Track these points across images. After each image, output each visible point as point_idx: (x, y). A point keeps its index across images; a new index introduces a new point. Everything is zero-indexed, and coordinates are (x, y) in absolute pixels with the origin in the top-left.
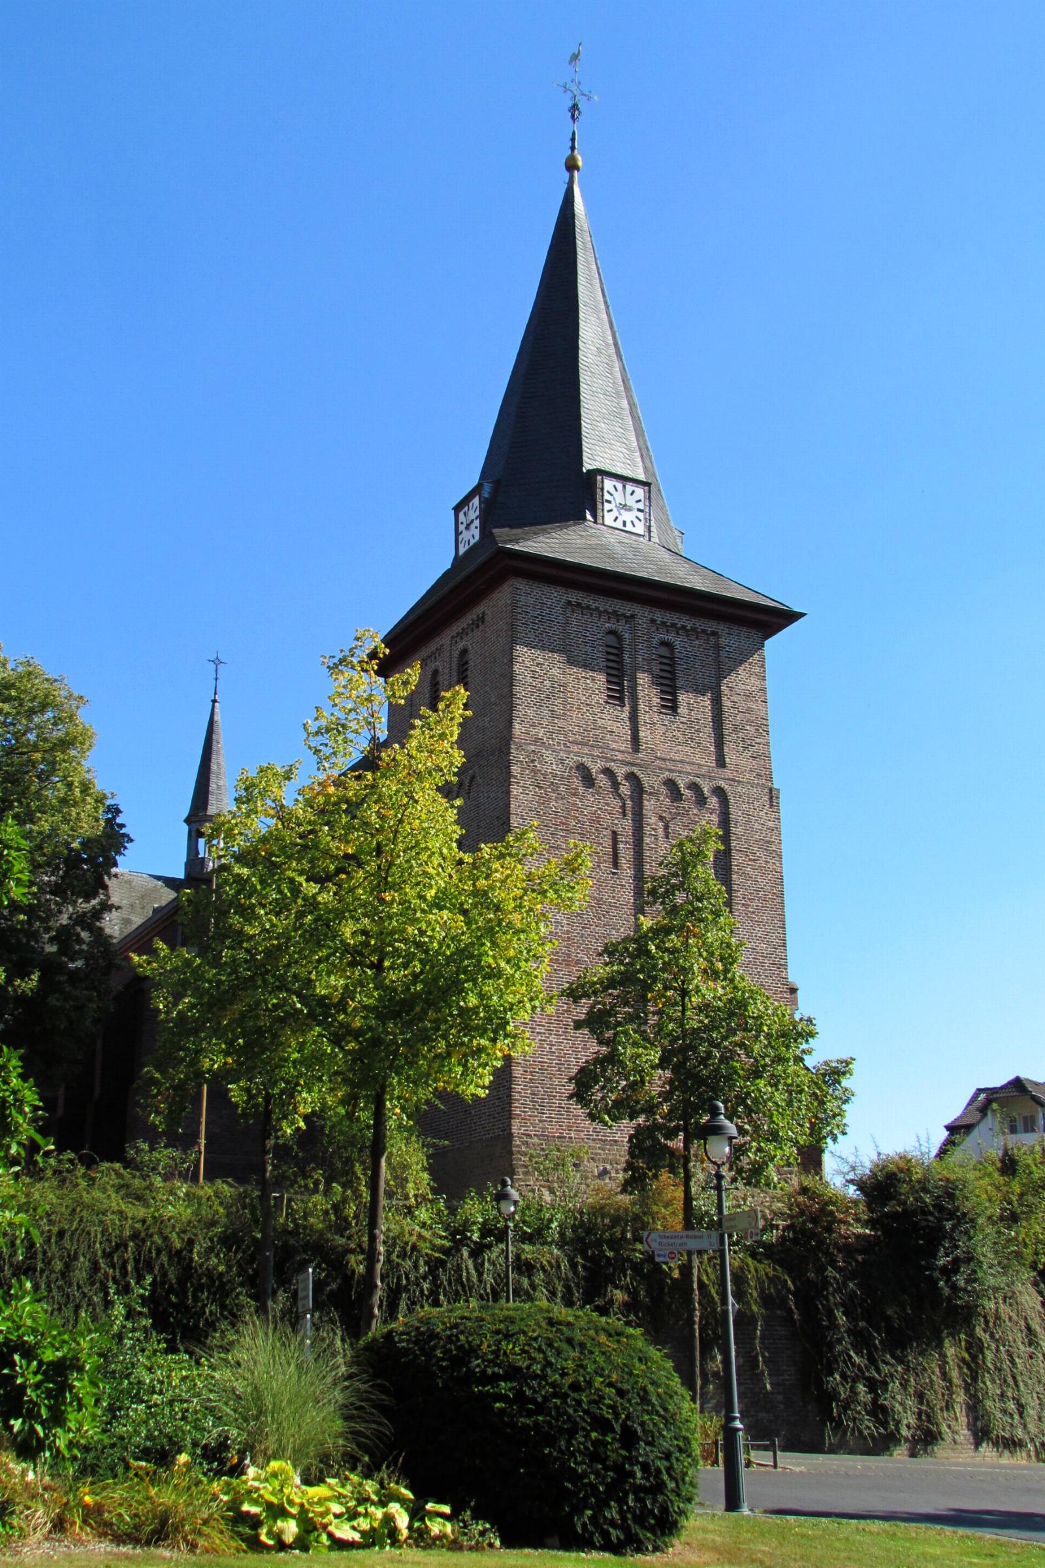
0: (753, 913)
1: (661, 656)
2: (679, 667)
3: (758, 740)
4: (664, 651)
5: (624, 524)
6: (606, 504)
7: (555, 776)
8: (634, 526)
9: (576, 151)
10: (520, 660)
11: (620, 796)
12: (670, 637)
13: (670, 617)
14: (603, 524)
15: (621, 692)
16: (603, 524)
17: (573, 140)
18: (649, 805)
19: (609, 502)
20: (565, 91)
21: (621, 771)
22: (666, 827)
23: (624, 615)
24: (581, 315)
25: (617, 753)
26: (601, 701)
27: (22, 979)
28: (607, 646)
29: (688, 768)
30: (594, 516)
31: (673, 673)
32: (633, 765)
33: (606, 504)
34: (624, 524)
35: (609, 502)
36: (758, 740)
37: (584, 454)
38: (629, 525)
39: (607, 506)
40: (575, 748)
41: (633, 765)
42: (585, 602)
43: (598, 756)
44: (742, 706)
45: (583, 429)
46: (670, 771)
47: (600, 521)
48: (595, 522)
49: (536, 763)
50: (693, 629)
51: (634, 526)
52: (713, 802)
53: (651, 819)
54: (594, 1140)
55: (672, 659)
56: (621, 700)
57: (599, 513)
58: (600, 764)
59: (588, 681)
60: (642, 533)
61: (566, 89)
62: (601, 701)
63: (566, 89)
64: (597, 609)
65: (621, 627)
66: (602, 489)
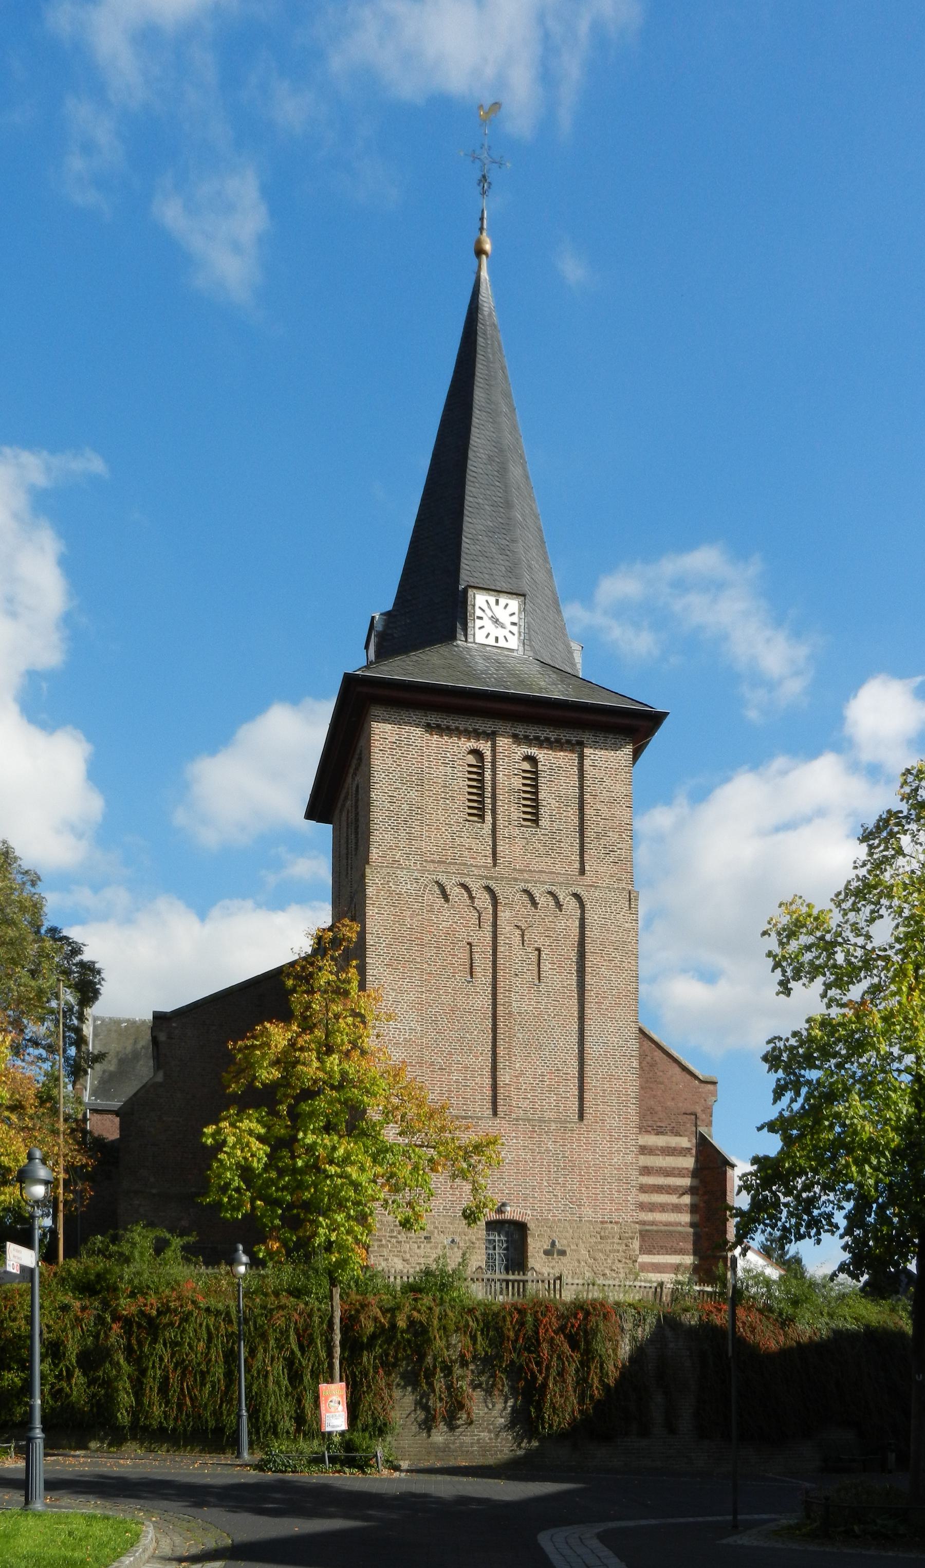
0: (606, 1009)
1: (524, 771)
2: (541, 780)
3: (619, 846)
4: (526, 766)
5: (497, 639)
6: (477, 621)
7: (410, 895)
8: (507, 640)
9: (485, 234)
10: (377, 786)
11: (475, 908)
12: (533, 751)
13: (533, 731)
14: (474, 642)
15: (482, 809)
16: (474, 642)
17: (482, 219)
18: (504, 915)
19: (480, 618)
20: (473, 162)
21: (476, 886)
22: (523, 936)
23: (484, 732)
24: (475, 421)
25: (473, 869)
26: (461, 820)
27: (312, 1100)
28: (470, 766)
29: (544, 877)
30: (466, 635)
31: (536, 787)
32: (491, 878)
33: (477, 621)
34: (497, 639)
35: (480, 618)
36: (619, 846)
37: (462, 571)
38: (501, 640)
39: (478, 623)
40: (431, 867)
41: (491, 878)
42: (444, 723)
43: (454, 873)
44: (605, 811)
45: (464, 545)
46: (527, 881)
47: (470, 639)
48: (466, 641)
49: (391, 884)
50: (558, 741)
51: (507, 640)
52: (571, 905)
53: (506, 929)
54: (444, 1216)
55: (536, 773)
56: (482, 817)
57: (470, 632)
58: (456, 879)
59: (448, 802)
60: (516, 648)
61: (475, 158)
62: (461, 820)
63: (475, 158)
64: (457, 729)
65: (485, 747)
66: (474, 606)
